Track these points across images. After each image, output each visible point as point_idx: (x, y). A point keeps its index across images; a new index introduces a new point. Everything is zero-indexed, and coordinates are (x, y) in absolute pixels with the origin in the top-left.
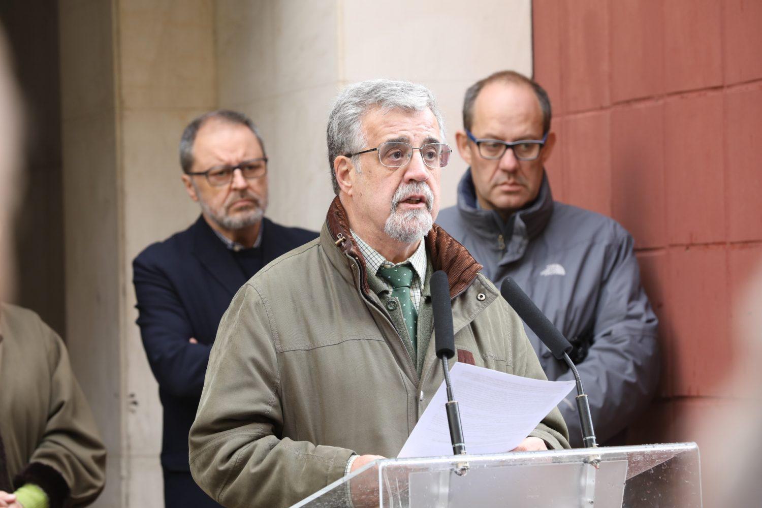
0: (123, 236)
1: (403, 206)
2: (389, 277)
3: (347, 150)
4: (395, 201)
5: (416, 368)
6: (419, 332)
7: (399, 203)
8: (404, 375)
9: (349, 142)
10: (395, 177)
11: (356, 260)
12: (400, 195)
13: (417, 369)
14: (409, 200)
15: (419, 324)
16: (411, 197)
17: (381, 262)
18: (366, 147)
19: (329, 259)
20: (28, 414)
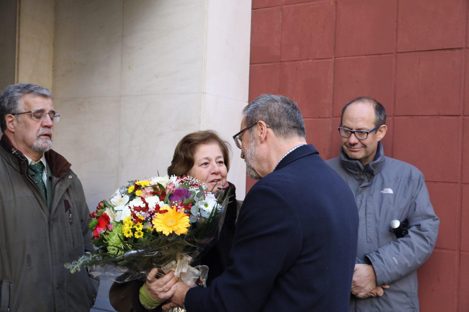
0: (206, 131)
1: (42, 137)
2: (34, 169)
3: (13, 112)
4: (38, 135)
5: (47, 206)
6: (47, 193)
7: (40, 135)
8: (43, 213)
9: (15, 108)
10: (38, 125)
11: (25, 160)
12: (40, 133)
13: (48, 207)
14: (46, 135)
15: (48, 195)
16: (165, 293)
17: (31, 161)
18: (24, 111)
19: (7, 161)
20: (34, 157)
